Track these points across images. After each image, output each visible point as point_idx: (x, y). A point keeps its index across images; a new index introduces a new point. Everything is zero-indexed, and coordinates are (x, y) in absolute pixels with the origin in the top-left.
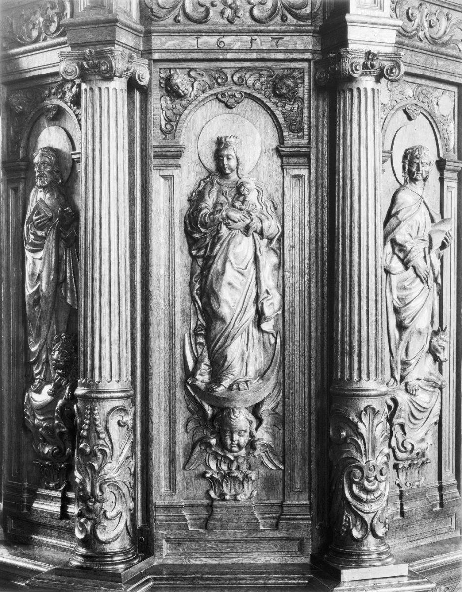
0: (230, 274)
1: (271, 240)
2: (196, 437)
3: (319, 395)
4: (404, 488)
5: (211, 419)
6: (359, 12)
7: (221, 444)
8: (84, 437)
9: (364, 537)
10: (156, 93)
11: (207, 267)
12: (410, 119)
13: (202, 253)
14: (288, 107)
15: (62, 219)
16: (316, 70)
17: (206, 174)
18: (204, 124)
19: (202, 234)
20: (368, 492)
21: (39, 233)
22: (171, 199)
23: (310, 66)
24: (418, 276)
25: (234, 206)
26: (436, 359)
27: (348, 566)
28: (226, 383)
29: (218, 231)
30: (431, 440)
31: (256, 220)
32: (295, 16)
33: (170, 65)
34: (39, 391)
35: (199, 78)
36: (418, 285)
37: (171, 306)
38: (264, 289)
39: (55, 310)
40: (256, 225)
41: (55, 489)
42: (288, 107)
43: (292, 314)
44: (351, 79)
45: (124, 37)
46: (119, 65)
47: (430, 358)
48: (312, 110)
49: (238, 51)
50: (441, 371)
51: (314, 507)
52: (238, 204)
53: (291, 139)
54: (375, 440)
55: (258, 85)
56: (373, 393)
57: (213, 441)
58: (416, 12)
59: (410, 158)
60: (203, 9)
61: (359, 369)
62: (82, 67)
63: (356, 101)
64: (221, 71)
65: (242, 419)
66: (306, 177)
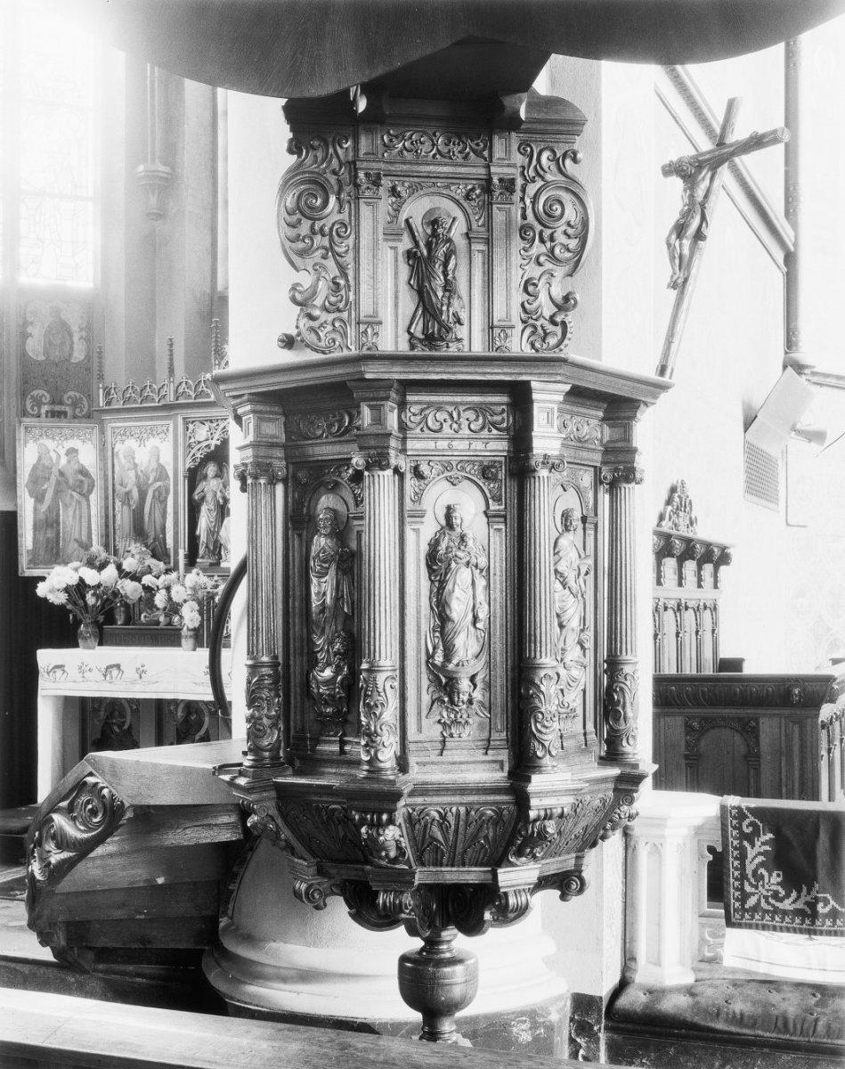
0: (457, 593)
1: (482, 571)
2: (434, 697)
3: (513, 669)
4: (563, 732)
5: (445, 685)
6: (539, 429)
7: (452, 702)
8: (369, 696)
9: (544, 756)
10: (408, 476)
11: (441, 588)
12: (565, 490)
13: (438, 578)
14: (492, 485)
15: (341, 556)
16: (510, 462)
17: (439, 528)
18: (438, 495)
19: (437, 565)
20: (546, 727)
21: (324, 565)
22: (418, 545)
23: (506, 460)
24: (572, 593)
25: (459, 548)
26: (583, 648)
27: (534, 773)
28: (455, 661)
29: (449, 565)
30: (579, 701)
31: (473, 557)
32: (497, 429)
33: (417, 458)
34: (323, 671)
35: (436, 466)
36: (572, 599)
37: (418, 612)
38: (478, 601)
39: (335, 617)
40: (474, 561)
41: (335, 736)
42: (492, 485)
43: (495, 617)
44: (535, 471)
45: (393, 443)
46: (393, 462)
47: (579, 647)
48: (508, 488)
49: (461, 451)
50: (584, 656)
51: (510, 740)
52: (462, 547)
53: (494, 506)
54: (550, 697)
55: (473, 472)
56: (548, 666)
57: (446, 699)
58: (569, 423)
59: (566, 516)
60: (438, 424)
61: (541, 651)
62: (367, 462)
63: (537, 484)
64: (449, 462)
65: (464, 685)
66: (504, 530)
